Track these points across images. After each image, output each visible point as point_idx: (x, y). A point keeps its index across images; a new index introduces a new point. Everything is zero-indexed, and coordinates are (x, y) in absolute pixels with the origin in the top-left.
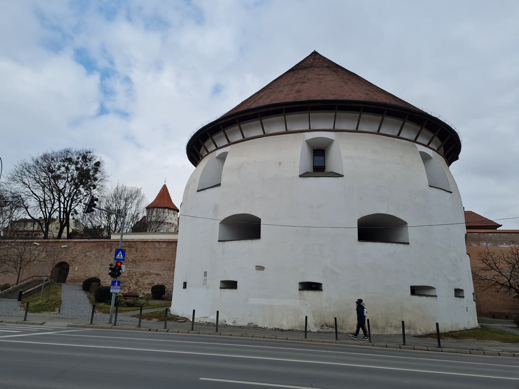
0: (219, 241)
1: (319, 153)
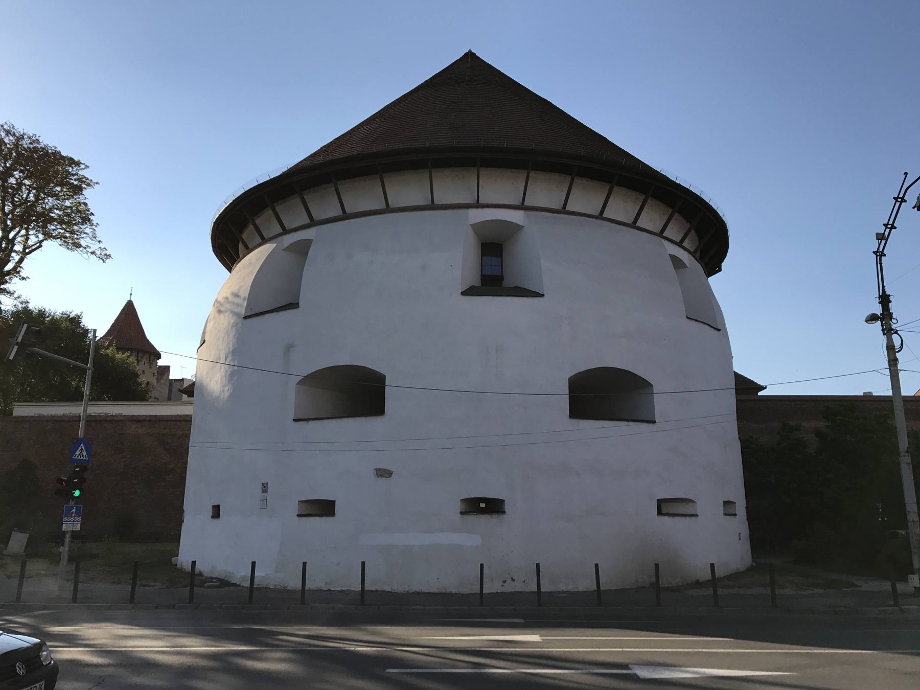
0: (294, 420)
1: (494, 247)
